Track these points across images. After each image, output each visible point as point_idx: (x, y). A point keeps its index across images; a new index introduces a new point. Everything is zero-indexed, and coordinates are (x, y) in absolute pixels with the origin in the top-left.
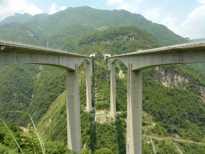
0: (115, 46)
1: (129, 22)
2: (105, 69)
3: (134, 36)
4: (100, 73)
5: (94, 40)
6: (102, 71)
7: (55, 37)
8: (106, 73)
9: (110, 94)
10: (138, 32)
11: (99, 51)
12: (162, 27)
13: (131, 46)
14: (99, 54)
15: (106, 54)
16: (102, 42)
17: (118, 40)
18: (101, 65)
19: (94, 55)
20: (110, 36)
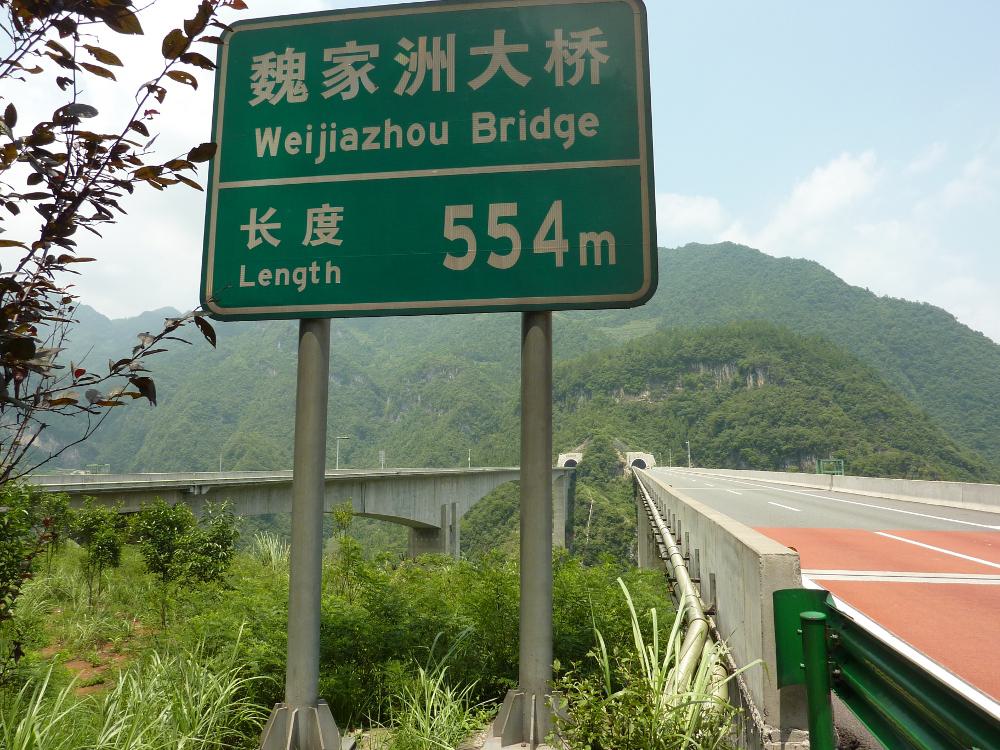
0: (675, 413)
1: (761, 297)
2: (621, 520)
3: (765, 370)
4: (599, 540)
5: (584, 385)
6: (611, 530)
7: (421, 374)
8: (626, 540)
9: (632, 633)
10: (783, 352)
11: (599, 440)
12: (929, 316)
13: (752, 415)
14: (600, 450)
15: (633, 450)
16: (618, 395)
17: (691, 386)
18: (605, 502)
19: (578, 457)
20: (656, 369)
